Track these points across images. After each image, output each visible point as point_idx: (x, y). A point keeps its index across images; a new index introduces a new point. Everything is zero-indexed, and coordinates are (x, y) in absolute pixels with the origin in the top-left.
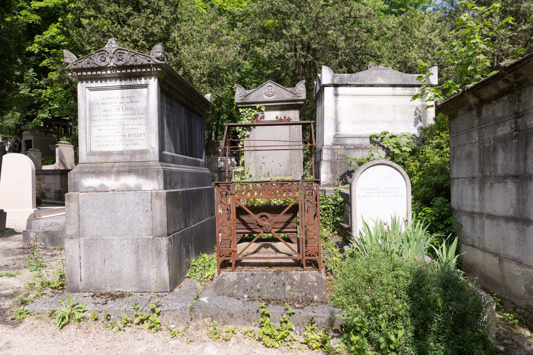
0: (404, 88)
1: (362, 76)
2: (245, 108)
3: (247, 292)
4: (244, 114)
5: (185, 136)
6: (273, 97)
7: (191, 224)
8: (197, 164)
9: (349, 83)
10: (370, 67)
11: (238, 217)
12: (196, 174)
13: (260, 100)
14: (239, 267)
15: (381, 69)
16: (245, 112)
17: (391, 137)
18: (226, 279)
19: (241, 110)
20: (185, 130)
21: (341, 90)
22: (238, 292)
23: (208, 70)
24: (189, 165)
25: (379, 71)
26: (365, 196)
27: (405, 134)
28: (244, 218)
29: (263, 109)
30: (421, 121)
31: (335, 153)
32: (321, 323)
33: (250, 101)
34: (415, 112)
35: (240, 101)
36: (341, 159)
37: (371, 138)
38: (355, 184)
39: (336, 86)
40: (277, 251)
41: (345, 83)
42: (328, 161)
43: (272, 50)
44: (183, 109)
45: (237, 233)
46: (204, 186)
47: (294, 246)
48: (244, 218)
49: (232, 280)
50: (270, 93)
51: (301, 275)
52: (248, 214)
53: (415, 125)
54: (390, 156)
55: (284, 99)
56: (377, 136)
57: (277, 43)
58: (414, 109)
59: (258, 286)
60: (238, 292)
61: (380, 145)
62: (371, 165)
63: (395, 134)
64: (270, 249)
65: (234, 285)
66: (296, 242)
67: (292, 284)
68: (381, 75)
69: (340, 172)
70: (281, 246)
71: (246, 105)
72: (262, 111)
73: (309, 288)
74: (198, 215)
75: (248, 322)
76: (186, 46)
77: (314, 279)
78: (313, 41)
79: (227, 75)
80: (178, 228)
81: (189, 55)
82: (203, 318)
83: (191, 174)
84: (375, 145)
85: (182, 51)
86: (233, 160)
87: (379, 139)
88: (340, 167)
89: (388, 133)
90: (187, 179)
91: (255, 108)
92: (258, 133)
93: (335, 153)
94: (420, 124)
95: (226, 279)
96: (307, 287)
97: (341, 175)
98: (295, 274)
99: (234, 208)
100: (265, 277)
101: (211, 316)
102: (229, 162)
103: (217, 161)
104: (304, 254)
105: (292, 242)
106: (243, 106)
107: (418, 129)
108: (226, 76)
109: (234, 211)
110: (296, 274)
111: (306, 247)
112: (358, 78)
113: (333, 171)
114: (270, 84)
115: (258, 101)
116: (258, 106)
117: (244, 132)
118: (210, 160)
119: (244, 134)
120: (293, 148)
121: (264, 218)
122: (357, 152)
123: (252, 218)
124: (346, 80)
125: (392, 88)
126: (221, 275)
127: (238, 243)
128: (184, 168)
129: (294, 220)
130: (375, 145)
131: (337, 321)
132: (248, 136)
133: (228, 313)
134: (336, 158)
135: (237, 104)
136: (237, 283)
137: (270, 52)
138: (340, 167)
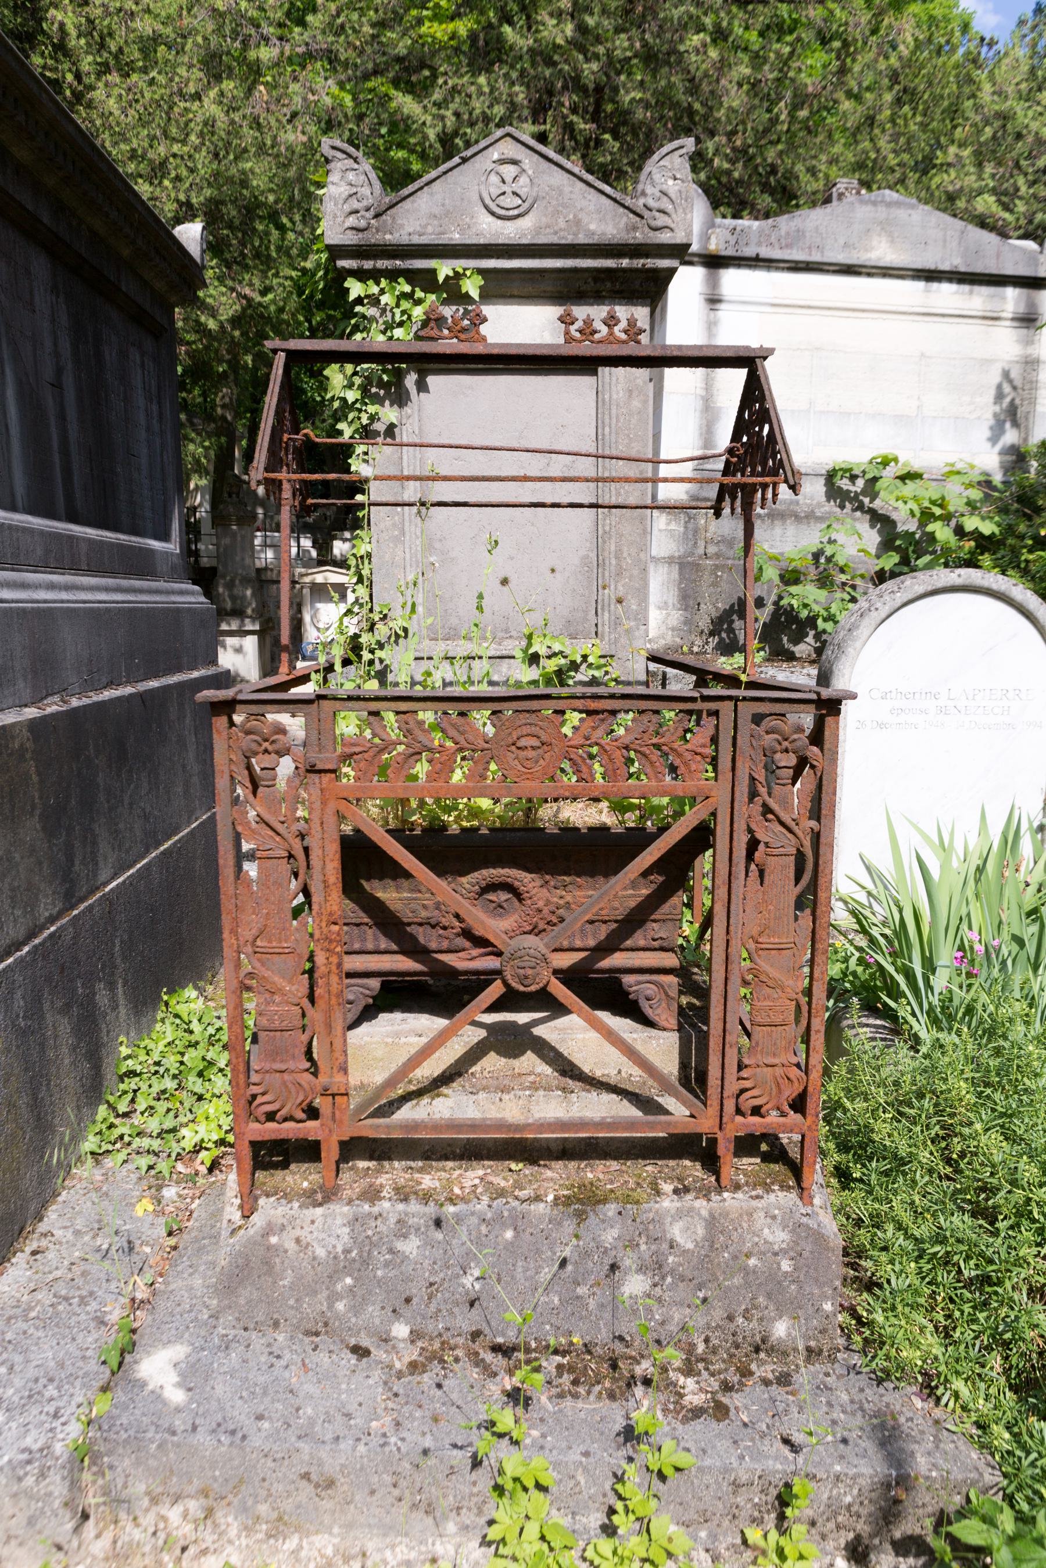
0: (966, 288)
1: (812, 228)
2: (375, 275)
3: (406, 1311)
4: (372, 312)
5: (62, 417)
6: (526, 223)
7: (103, 877)
8: (139, 565)
9: (765, 252)
10: (841, 196)
11: (351, 888)
12: (132, 615)
13: (456, 237)
14: (362, 1164)
15: (889, 205)
16: (375, 301)
17: (904, 478)
18: (291, 1246)
19: (355, 289)
20: (57, 385)
21: (731, 279)
22: (356, 1310)
23: (208, 192)
25: (882, 212)
26: (881, 725)
27: (959, 466)
28: (387, 893)
29: (471, 287)
30: (1015, 424)
31: (696, 531)
32: (833, 1509)
33: (405, 240)
34: (999, 387)
35: (350, 239)
36: (717, 555)
37: (830, 477)
38: (846, 672)
39: (714, 262)
40: (568, 1069)
41: (749, 251)
42: (670, 560)
43: (457, 114)
44: (40, 267)
45: (350, 975)
46: (179, 669)
47: (662, 1048)
48: (387, 893)
49: (321, 1252)
50: (509, 201)
51: (712, 1222)
53: (994, 439)
54: (897, 549)
55: (582, 239)
56: (856, 472)
57: (482, 80)
58: (996, 378)
59: (468, 1281)
60: (356, 1310)
61: (861, 507)
62: (920, 589)
63: (916, 466)
64: (529, 1060)
65: (333, 1277)
66: (673, 1023)
67: (656, 1268)
68: (886, 227)
69: (710, 608)
70: (576, 1033)
71: (382, 264)
72: (466, 298)
73: (747, 1284)
74: (146, 817)
75: (420, 1514)
76: (114, 78)
77: (779, 1237)
78: (623, 77)
79: (281, 228)
80: (14, 931)
81: (124, 111)
82: (155, 1501)
83: (97, 618)
84: (842, 507)
85: (99, 94)
86: (306, 543)
87: (860, 483)
88: (715, 584)
89: (896, 460)
90: (71, 644)
91: (426, 280)
92: (447, 404)
93: (696, 531)
94: (1011, 437)
95: (291, 1246)
96: (737, 1280)
97: (714, 615)
98: (679, 1214)
99: (333, 849)
100: (509, 1234)
101: (205, 1493)
102: (294, 551)
103: (253, 545)
104: (730, 1106)
105: (648, 1022)
106: (368, 265)
107: (1003, 452)
108: (275, 234)
109: (328, 865)
110: (680, 1212)
111: (741, 1067)
112: (800, 233)
113: (688, 600)
114: (508, 149)
115: (444, 240)
116: (444, 269)
117: (372, 409)
118: (227, 541)
119: (373, 418)
120: (611, 494)
121: (503, 896)
122: (778, 531)
123: (426, 895)
124: (754, 239)
125: (921, 285)
126: (258, 1220)
127: (352, 1027)
128: (51, 587)
129: (666, 908)
130: (842, 507)
131: (922, 1496)
132: (390, 430)
133: (306, 1476)
134: (701, 551)
135: (336, 252)
136: (358, 1260)
137: (450, 121)
138: (715, 584)
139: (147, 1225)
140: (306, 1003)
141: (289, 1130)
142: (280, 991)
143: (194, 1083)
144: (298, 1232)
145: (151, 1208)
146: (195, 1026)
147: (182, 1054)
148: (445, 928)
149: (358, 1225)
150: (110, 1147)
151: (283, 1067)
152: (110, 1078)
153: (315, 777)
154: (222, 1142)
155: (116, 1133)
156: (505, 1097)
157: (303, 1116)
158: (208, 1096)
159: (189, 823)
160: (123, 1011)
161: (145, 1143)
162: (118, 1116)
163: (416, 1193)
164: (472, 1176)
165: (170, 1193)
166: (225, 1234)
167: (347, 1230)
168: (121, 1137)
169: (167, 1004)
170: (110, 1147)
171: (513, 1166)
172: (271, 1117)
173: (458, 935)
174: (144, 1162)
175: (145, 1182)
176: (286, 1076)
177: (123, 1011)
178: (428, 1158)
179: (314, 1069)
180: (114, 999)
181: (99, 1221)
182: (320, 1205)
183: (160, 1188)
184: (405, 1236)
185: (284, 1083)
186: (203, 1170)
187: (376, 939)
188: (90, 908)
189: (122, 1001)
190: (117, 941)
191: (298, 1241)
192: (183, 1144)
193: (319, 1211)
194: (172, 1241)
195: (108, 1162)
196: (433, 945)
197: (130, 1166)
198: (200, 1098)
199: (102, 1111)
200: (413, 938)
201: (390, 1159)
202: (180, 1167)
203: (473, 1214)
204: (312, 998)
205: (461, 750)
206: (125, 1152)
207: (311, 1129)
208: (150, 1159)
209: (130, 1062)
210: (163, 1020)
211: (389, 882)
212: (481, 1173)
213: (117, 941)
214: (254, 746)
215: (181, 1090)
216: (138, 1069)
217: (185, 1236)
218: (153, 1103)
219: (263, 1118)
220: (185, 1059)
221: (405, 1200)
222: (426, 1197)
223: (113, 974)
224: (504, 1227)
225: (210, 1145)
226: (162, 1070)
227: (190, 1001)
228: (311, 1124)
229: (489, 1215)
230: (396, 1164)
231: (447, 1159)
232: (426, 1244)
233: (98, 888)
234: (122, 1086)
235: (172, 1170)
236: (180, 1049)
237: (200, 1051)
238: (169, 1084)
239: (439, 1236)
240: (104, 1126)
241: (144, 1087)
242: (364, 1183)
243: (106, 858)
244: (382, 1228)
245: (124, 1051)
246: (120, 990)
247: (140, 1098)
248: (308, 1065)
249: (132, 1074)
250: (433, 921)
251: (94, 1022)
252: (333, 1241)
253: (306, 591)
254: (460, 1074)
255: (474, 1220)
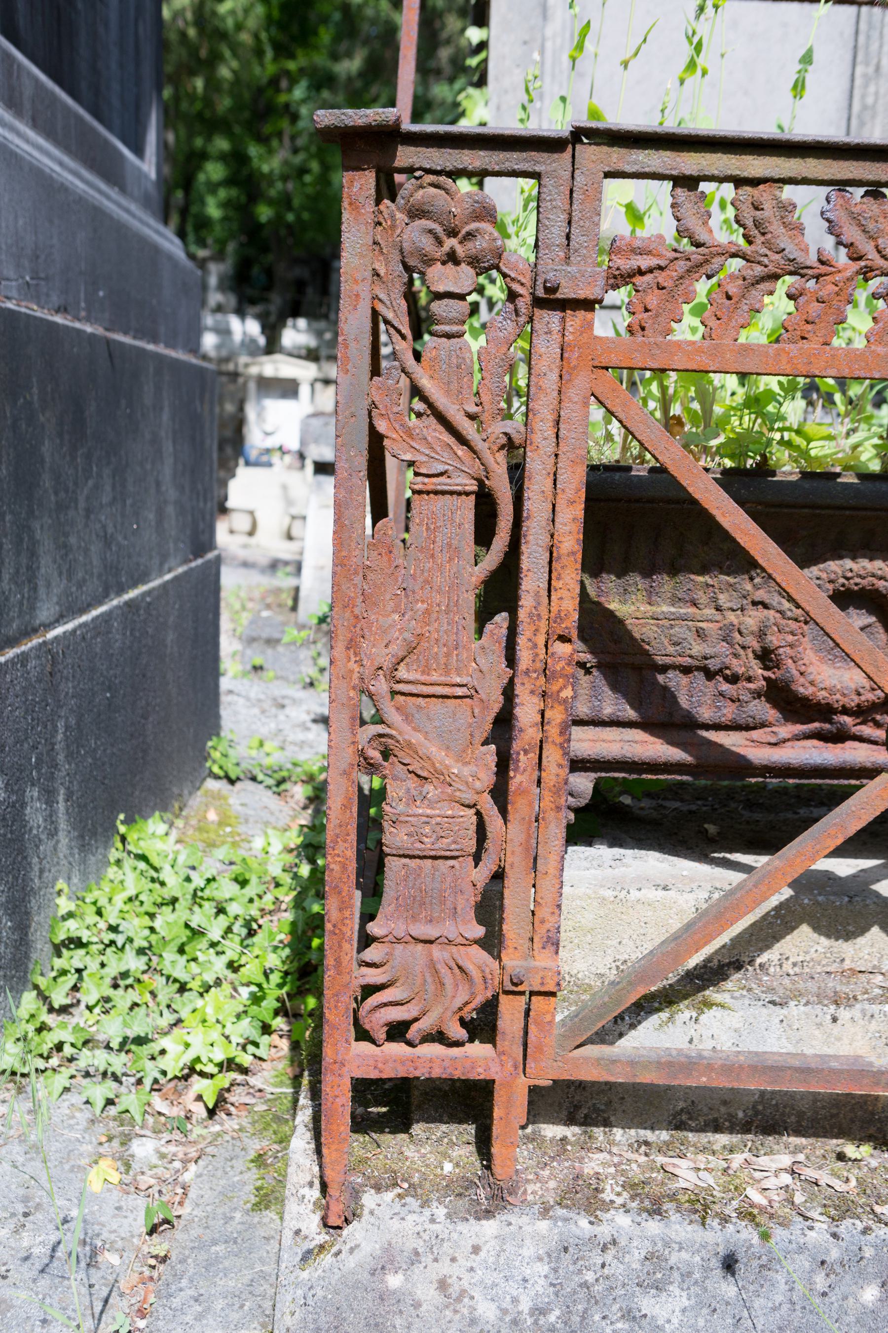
7: (44, 613)
8: (110, 170)
18: (428, 1294)
24: (57, 143)
49: (487, 1311)
52: (742, 563)
74: (107, 541)
95: (428, 1294)
99: (574, 483)
109: (555, 521)
139: (110, 1210)
140: (488, 805)
141: (429, 1061)
142: (443, 778)
143: (177, 966)
144: (444, 1268)
145: (115, 1177)
146: (167, 875)
147: (152, 916)
148: (734, 679)
149: (567, 1258)
150: (41, 1064)
151: (431, 932)
152: (41, 949)
153: (551, 319)
154: (229, 1065)
155: (50, 1039)
156: (844, 1014)
157: (461, 1033)
158: (195, 985)
159: (161, 574)
160: (63, 840)
161: (99, 1059)
162: (51, 1010)
163: (673, 1197)
164: (774, 1166)
165: (144, 1149)
166: (290, 1258)
167: (543, 1269)
168: (59, 1047)
169: (123, 839)
170: (41, 1064)
171: (851, 1150)
172: (397, 1031)
173: (757, 694)
174: (99, 1091)
175: (100, 1128)
176: (436, 951)
177: (63, 840)
178: (680, 1126)
179: (492, 942)
180: (51, 818)
181: (25, 1200)
182: (488, 1214)
183: (126, 1140)
184: (659, 1288)
185: (432, 965)
186: (200, 1111)
187: (595, 695)
188: (23, 658)
189: (63, 825)
190: (61, 724)
191: (443, 1285)
192: (164, 1063)
193: (490, 1227)
194: (158, 1245)
195: (41, 1087)
196: (705, 714)
197: (75, 1098)
198: (183, 988)
199: (29, 998)
200: (668, 695)
201: (607, 1123)
202: (158, 1103)
203: (802, 1249)
204: (500, 793)
205: (867, 273)
206: (66, 1072)
207: (476, 1059)
208: (108, 1088)
209: (71, 924)
210: (118, 862)
211: (635, 579)
212: (786, 1160)
213: (61, 724)
214: (427, 244)
215: (156, 973)
216: (85, 936)
217: (178, 1234)
218: (110, 992)
219: (381, 1035)
220: (158, 924)
221: (656, 1211)
222: (700, 1208)
223: (51, 777)
224: (862, 1278)
225: (210, 1069)
226: (120, 940)
227: (154, 835)
228: (478, 1050)
229: (834, 1254)
230: (618, 1133)
231: (717, 1128)
232: (700, 1304)
233: (35, 631)
234: (58, 963)
235: (147, 1109)
236: (148, 907)
237: (182, 912)
238: (134, 963)
239: (728, 1289)
240: (31, 1028)
241: (93, 965)
242: (562, 1169)
243: (48, 585)
244: (616, 1269)
245: (64, 905)
246: (61, 806)
247: (87, 983)
248: (480, 931)
249: (77, 943)
250: (713, 664)
251: (21, 851)
252: (513, 1288)
253: (252, 386)
254: (738, 966)
255: (804, 1262)
